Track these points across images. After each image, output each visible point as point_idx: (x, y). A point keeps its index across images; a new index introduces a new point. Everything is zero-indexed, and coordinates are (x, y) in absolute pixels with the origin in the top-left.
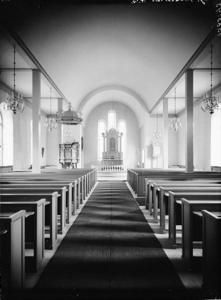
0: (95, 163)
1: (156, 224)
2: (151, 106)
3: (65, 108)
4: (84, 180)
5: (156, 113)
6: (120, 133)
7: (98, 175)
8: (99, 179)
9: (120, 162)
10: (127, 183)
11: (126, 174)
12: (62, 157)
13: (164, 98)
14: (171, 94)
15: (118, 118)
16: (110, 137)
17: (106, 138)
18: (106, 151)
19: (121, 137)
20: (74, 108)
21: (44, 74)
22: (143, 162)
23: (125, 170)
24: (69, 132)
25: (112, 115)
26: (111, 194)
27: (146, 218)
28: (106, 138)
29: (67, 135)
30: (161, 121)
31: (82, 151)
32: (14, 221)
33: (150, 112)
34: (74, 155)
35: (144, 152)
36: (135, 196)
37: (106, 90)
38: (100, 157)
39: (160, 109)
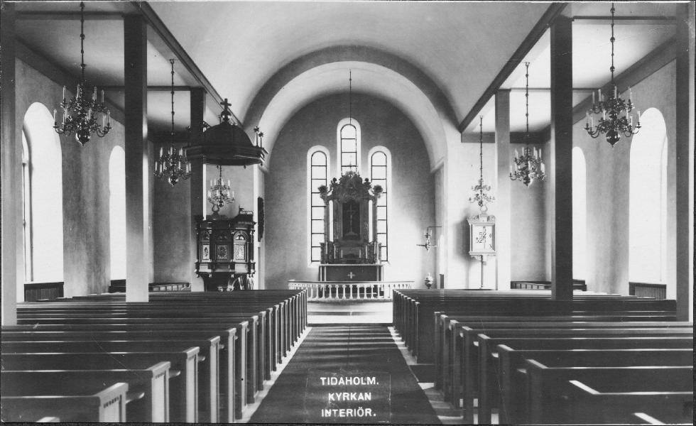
0: (298, 275)
1: (458, 418)
2: (464, 108)
3: (211, 117)
4: (267, 321)
5: (477, 129)
6: (374, 184)
7: (310, 308)
8: (312, 319)
9: (373, 273)
10: (392, 329)
11: (389, 307)
12: (206, 258)
13: (497, 92)
14: (515, 80)
15: (369, 140)
16: (344, 196)
17: (331, 203)
18: (331, 239)
19: (375, 200)
20: (238, 110)
21: (154, 27)
22: (442, 272)
23: (389, 295)
24: (223, 184)
25: (349, 132)
26: (346, 344)
27: (434, 407)
28: (331, 203)
29: (218, 194)
30: (491, 151)
31: (259, 241)
32: (106, 405)
33: (461, 127)
34: (239, 254)
35: (448, 239)
36: (411, 362)
37: (330, 61)
38: (312, 262)
39: (487, 119)
